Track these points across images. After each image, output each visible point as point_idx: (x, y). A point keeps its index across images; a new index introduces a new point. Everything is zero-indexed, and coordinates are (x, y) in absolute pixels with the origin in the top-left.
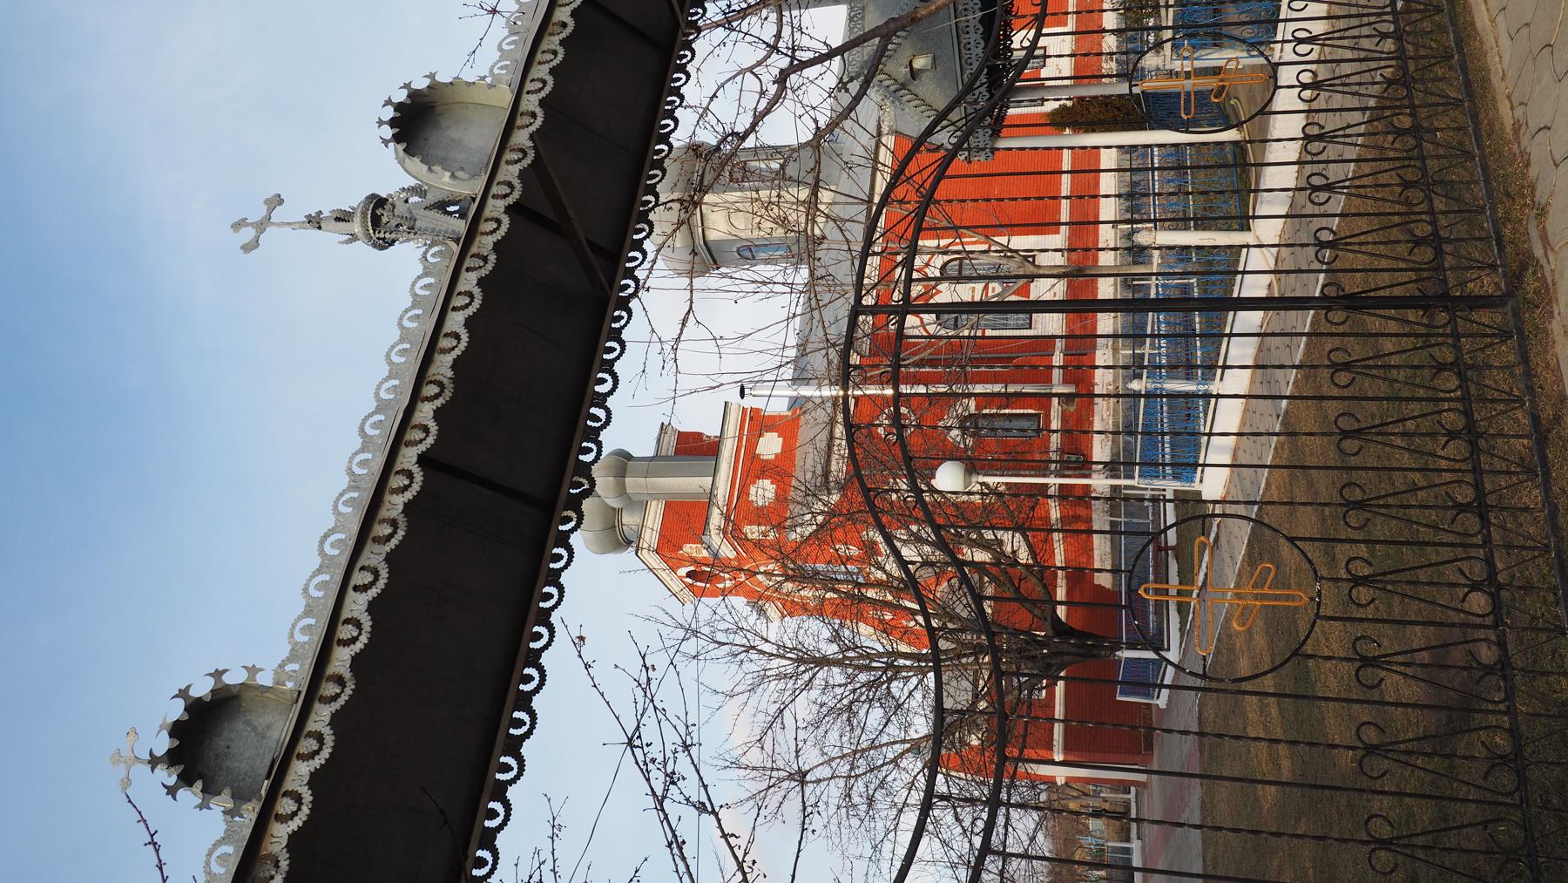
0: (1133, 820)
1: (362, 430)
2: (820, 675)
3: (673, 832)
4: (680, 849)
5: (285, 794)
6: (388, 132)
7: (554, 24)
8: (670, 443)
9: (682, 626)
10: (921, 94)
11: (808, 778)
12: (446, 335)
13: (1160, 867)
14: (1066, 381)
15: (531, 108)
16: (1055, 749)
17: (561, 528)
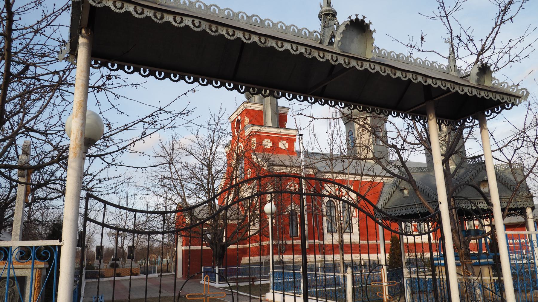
0: (131, 278)
1: (254, 16)
2: (206, 167)
3: (131, 126)
4: (125, 129)
5: (123, 4)
6: (354, 18)
7: (395, 71)
8: (283, 111)
9: (219, 119)
10: (395, 193)
11: (171, 165)
12: (282, 43)
13: (148, 283)
14: (310, 245)
15: (364, 65)
16: (186, 247)
17: (227, 83)
